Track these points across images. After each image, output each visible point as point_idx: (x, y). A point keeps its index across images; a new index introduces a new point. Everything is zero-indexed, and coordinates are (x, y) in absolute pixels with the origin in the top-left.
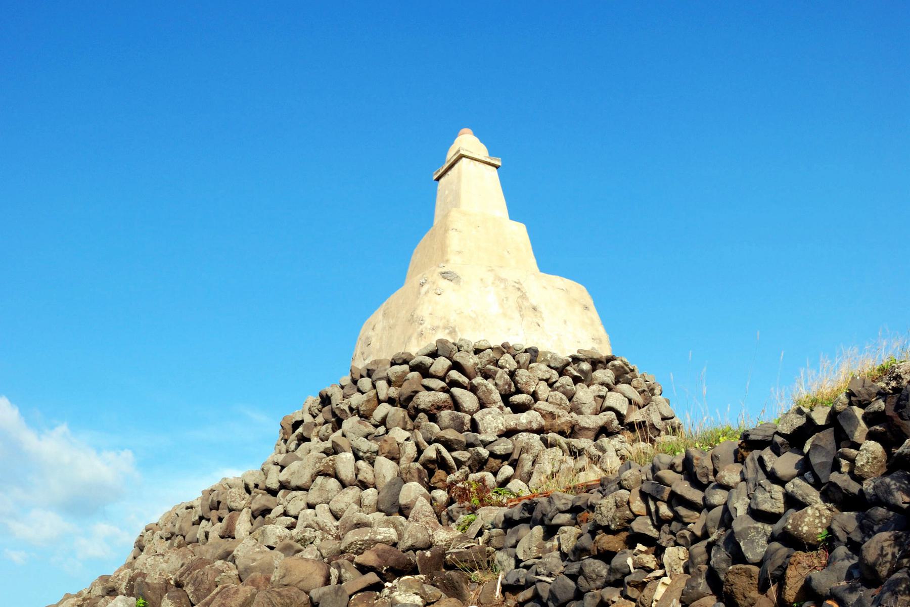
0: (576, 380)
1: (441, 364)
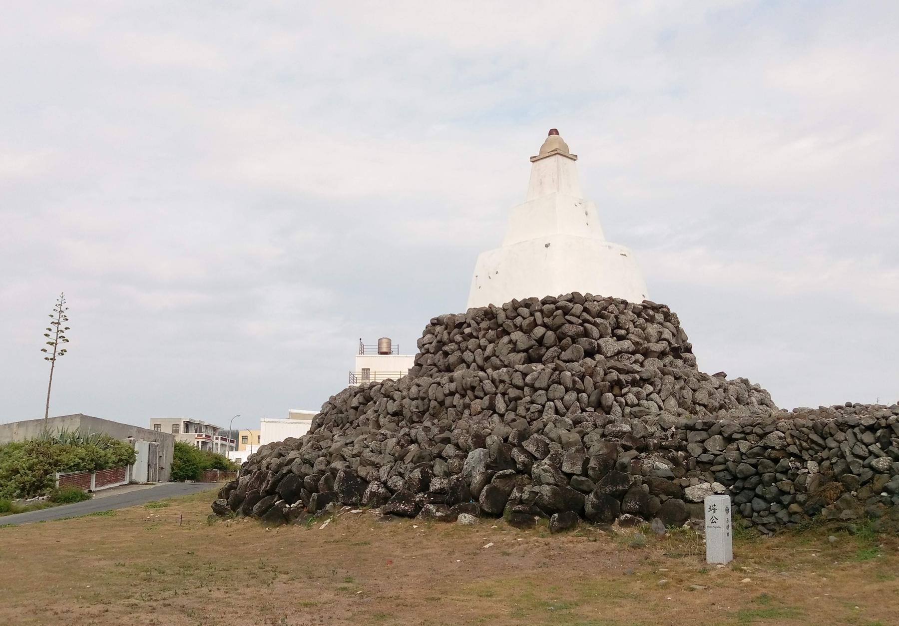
0: (647, 320)
1: (578, 309)
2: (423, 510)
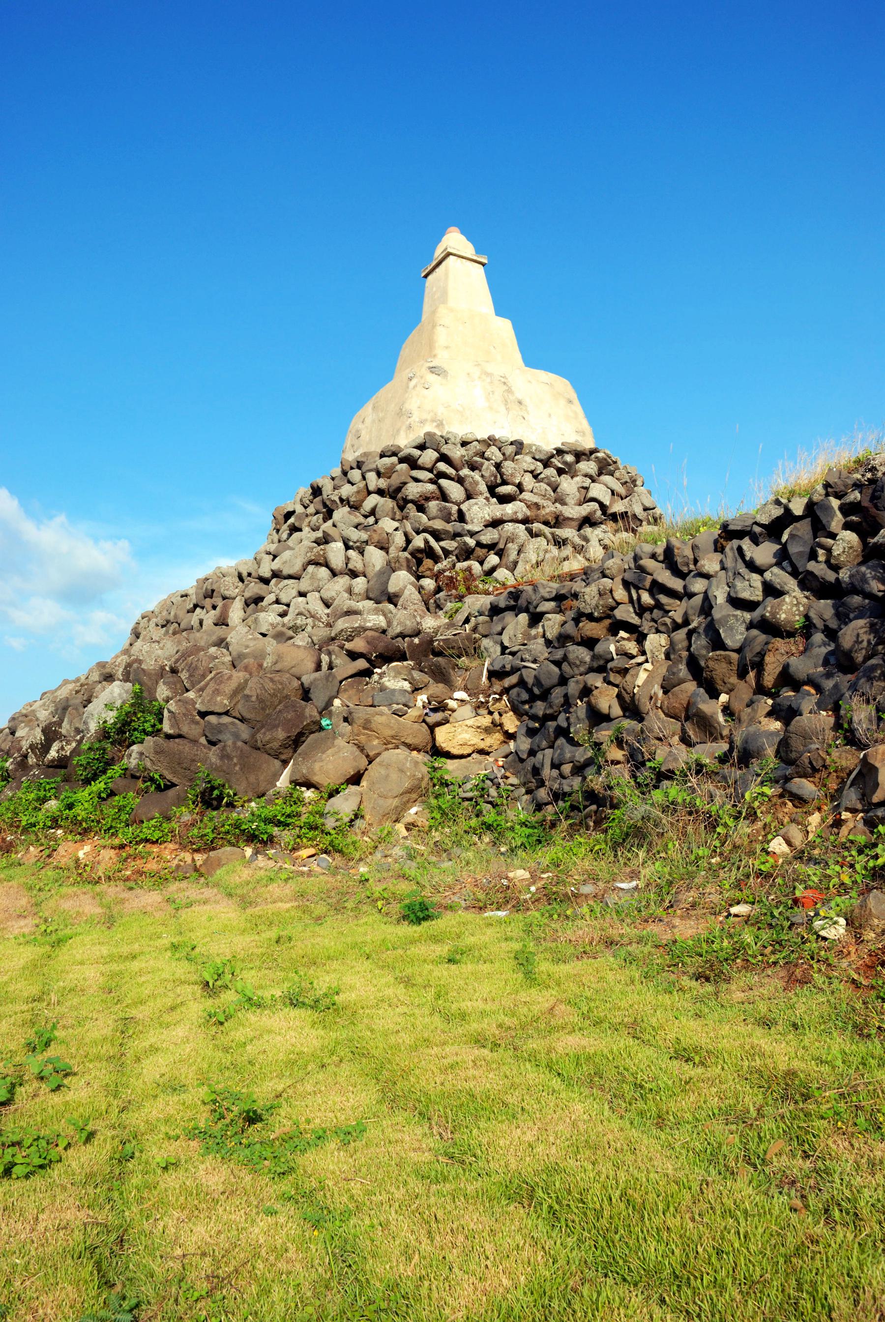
0: (560, 472)
1: (429, 457)
2: (237, 768)
